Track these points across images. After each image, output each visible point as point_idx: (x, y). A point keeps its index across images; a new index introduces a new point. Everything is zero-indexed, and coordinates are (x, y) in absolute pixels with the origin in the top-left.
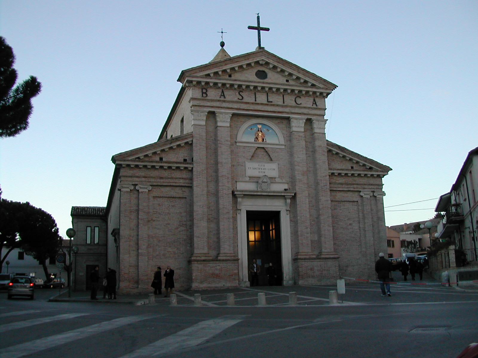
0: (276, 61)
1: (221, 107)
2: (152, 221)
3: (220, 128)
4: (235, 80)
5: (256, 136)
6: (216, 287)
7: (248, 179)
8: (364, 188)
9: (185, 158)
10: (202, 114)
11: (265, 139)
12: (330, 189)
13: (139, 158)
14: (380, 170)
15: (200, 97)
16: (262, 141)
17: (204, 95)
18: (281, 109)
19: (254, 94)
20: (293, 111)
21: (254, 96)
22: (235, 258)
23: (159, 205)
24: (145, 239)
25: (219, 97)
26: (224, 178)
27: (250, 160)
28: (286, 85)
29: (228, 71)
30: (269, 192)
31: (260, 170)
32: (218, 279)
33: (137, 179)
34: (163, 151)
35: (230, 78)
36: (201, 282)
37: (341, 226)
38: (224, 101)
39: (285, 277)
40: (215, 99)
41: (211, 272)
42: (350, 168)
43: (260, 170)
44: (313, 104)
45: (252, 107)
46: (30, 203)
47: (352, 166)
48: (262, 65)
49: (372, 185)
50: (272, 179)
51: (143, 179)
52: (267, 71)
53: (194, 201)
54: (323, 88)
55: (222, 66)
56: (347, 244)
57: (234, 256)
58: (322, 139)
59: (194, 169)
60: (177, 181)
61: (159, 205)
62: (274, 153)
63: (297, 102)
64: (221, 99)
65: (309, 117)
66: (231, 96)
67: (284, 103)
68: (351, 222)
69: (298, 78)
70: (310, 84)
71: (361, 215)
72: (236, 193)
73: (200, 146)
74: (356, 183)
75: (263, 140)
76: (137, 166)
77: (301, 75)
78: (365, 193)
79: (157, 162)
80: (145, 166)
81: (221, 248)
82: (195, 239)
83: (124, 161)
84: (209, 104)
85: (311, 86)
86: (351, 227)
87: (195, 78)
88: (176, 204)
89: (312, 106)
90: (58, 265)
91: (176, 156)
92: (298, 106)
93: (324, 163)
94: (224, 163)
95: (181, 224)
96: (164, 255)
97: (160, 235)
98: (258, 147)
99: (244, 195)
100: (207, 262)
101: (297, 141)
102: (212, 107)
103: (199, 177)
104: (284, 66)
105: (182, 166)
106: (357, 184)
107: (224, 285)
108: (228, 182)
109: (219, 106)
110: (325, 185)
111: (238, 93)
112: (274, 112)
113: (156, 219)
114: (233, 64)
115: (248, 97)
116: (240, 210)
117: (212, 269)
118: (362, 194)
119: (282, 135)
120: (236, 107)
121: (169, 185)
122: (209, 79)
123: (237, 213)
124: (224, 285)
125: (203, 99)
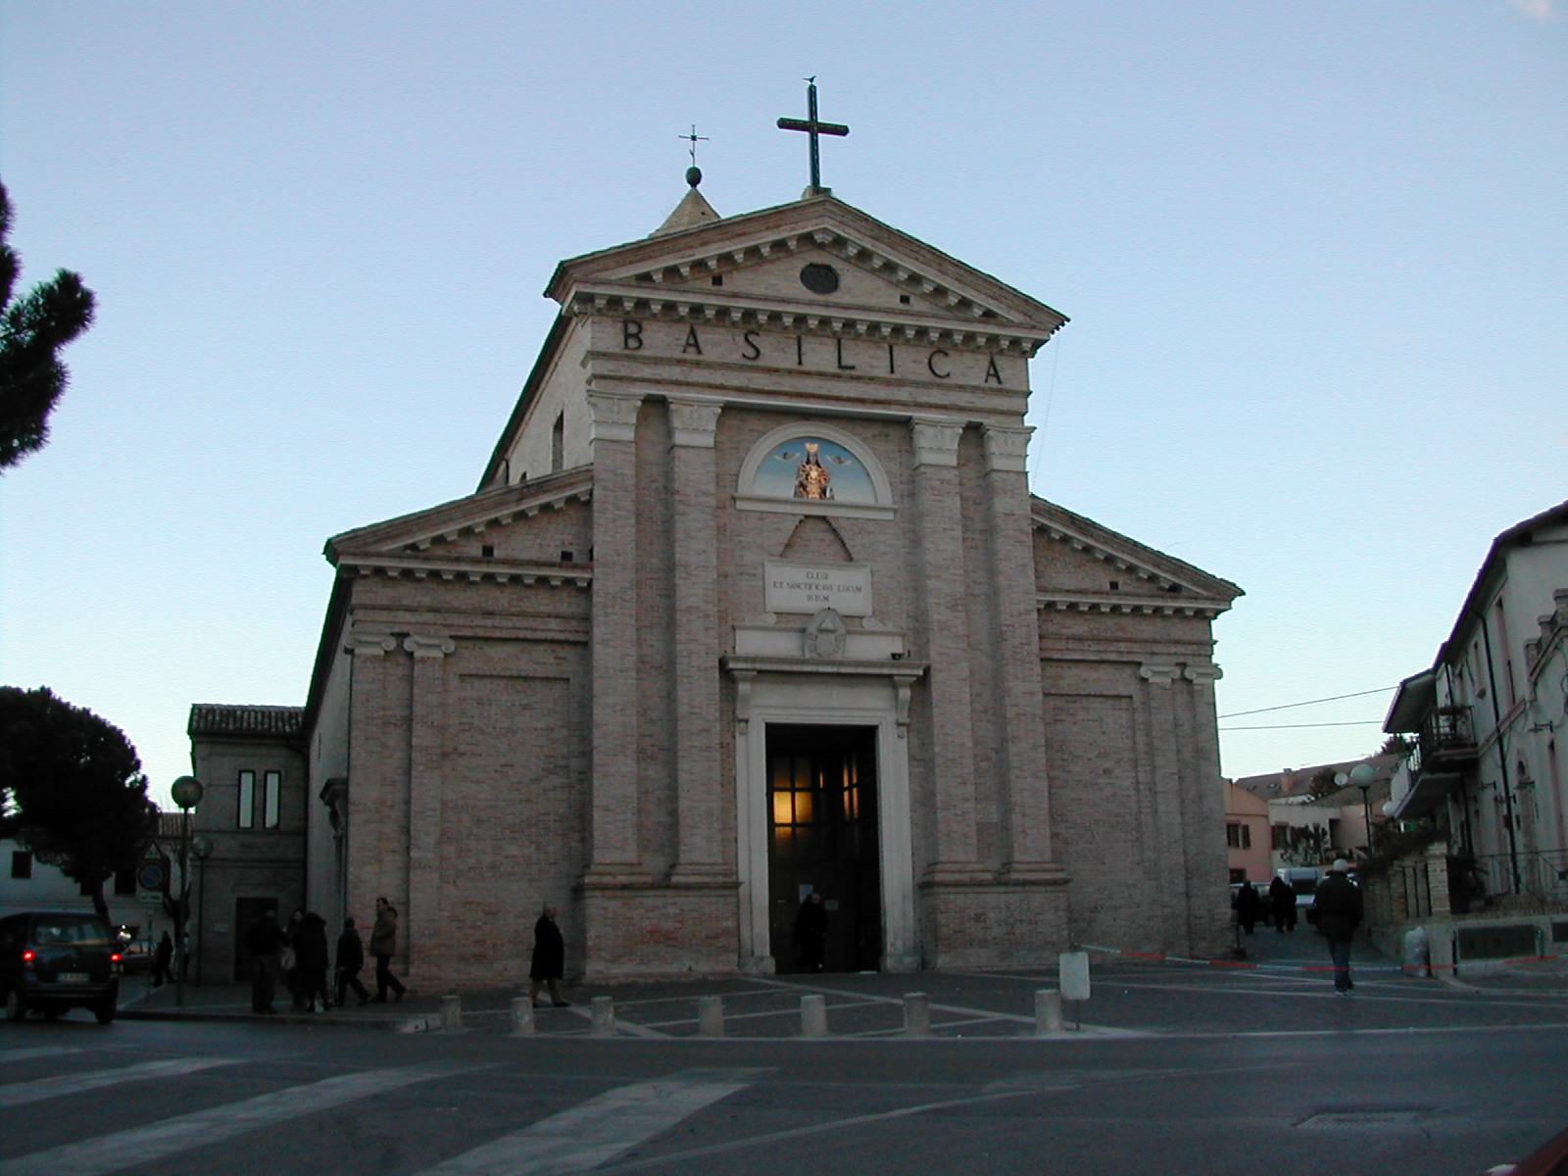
1: (688, 384)
4: (735, 296)
5: (801, 479)
6: (662, 975)
7: (771, 620)
8: (1153, 654)
9: (565, 549)
10: (624, 404)
11: (831, 490)
13: (414, 547)
14: (1204, 593)
16: (821, 497)
17: (633, 343)
18: (883, 393)
20: (922, 399)
23: (480, 703)
28: (902, 313)
29: (713, 264)
33: (408, 617)
34: (494, 524)
35: (716, 288)
36: (615, 959)
38: (698, 364)
42: (1108, 587)
44: (988, 375)
45: (788, 384)
47: (1115, 580)
48: (821, 246)
49: (1177, 642)
51: (428, 617)
52: (837, 265)
54: (1019, 326)
55: (692, 247)
58: (1016, 491)
60: (538, 623)
63: (937, 372)
67: (892, 372)
69: (940, 291)
70: (978, 312)
71: (1141, 739)
72: (731, 665)
74: (1128, 635)
75: (824, 492)
76: (407, 574)
78: (1156, 669)
79: (474, 561)
83: (367, 555)
84: (647, 372)
85: (983, 318)
87: (602, 287)
92: (939, 381)
96: (493, 867)
98: (807, 517)
99: (760, 672)
102: (658, 382)
103: (610, 610)
104: (893, 252)
105: (557, 574)
106: (1130, 640)
107: (690, 969)
109: (681, 378)
110: (1024, 641)
111: (742, 338)
113: (468, 748)
115: (776, 352)
116: (747, 721)
117: (650, 914)
118: (1144, 672)
120: (736, 383)
121: (513, 636)
122: (648, 291)
125: (628, 357)
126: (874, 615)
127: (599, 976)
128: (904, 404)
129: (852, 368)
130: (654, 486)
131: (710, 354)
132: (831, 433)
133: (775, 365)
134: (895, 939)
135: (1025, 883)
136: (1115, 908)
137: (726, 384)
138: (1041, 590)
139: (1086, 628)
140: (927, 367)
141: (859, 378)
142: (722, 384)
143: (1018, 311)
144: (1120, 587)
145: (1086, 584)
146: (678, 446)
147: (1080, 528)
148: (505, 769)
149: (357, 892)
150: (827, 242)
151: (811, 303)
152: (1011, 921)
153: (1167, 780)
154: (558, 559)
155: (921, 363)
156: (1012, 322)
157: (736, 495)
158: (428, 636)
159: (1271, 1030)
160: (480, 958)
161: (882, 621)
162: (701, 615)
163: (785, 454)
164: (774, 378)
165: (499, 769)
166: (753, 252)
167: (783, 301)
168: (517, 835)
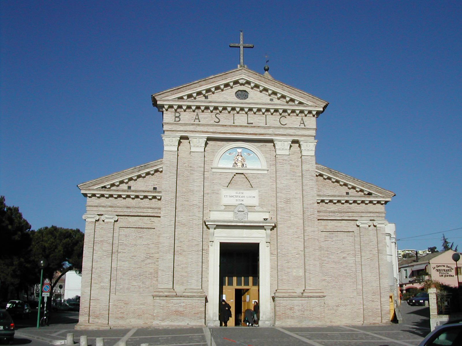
0: (257, 79)
1: (196, 131)
4: (210, 102)
5: (235, 161)
6: (178, 326)
7: (223, 208)
9: (154, 187)
10: (174, 139)
11: (246, 164)
12: (318, 218)
13: (104, 187)
14: (380, 195)
15: (172, 122)
16: (242, 167)
18: (262, 131)
22: (201, 295)
23: (126, 236)
26: (195, 208)
27: (226, 187)
29: (204, 92)
30: (245, 222)
31: (237, 198)
32: (181, 317)
33: (103, 209)
34: (130, 179)
35: (206, 100)
36: (163, 320)
37: (332, 260)
38: (198, 125)
39: (262, 317)
40: (189, 122)
41: (174, 308)
42: (345, 194)
43: (238, 198)
45: (229, 130)
46: (80, 229)
47: (348, 191)
49: (371, 212)
50: (251, 208)
51: (110, 209)
54: (311, 106)
55: (196, 87)
56: (340, 280)
57: (201, 293)
58: (310, 162)
60: (145, 210)
61: (126, 236)
62: (255, 179)
65: (296, 138)
66: (207, 120)
69: (283, 97)
70: (297, 102)
71: (357, 247)
74: (352, 211)
75: (243, 165)
76: (103, 196)
78: (362, 222)
79: (124, 191)
80: (355, 202)
83: (89, 190)
84: (182, 128)
85: (299, 105)
86: (345, 261)
87: (166, 102)
88: (143, 235)
91: (146, 184)
92: (283, 126)
93: (311, 188)
94: (195, 191)
96: (128, 289)
97: (124, 267)
98: (237, 173)
99: (217, 225)
100: (171, 298)
101: (281, 166)
102: (185, 131)
103: (167, 206)
104: (266, 84)
107: (188, 324)
108: (199, 211)
109: (193, 130)
110: (312, 213)
113: (122, 250)
114: (209, 85)
115: (225, 118)
118: (358, 223)
119: (265, 159)
120: (211, 130)
123: (209, 245)
124: (188, 324)
126: (261, 205)
127: (157, 325)
129: (252, 124)
132: (239, 144)
134: (263, 315)
135: (308, 297)
138: (319, 195)
139: (336, 209)
142: (207, 131)
144: (350, 193)
145: (337, 193)
150: (244, 83)
151: (237, 103)
152: (303, 310)
153: (366, 261)
155: (277, 121)
160: (122, 318)
161: (262, 208)
162: (197, 207)
163: (230, 153)
164: (225, 128)
166: (217, 88)
168: (136, 279)
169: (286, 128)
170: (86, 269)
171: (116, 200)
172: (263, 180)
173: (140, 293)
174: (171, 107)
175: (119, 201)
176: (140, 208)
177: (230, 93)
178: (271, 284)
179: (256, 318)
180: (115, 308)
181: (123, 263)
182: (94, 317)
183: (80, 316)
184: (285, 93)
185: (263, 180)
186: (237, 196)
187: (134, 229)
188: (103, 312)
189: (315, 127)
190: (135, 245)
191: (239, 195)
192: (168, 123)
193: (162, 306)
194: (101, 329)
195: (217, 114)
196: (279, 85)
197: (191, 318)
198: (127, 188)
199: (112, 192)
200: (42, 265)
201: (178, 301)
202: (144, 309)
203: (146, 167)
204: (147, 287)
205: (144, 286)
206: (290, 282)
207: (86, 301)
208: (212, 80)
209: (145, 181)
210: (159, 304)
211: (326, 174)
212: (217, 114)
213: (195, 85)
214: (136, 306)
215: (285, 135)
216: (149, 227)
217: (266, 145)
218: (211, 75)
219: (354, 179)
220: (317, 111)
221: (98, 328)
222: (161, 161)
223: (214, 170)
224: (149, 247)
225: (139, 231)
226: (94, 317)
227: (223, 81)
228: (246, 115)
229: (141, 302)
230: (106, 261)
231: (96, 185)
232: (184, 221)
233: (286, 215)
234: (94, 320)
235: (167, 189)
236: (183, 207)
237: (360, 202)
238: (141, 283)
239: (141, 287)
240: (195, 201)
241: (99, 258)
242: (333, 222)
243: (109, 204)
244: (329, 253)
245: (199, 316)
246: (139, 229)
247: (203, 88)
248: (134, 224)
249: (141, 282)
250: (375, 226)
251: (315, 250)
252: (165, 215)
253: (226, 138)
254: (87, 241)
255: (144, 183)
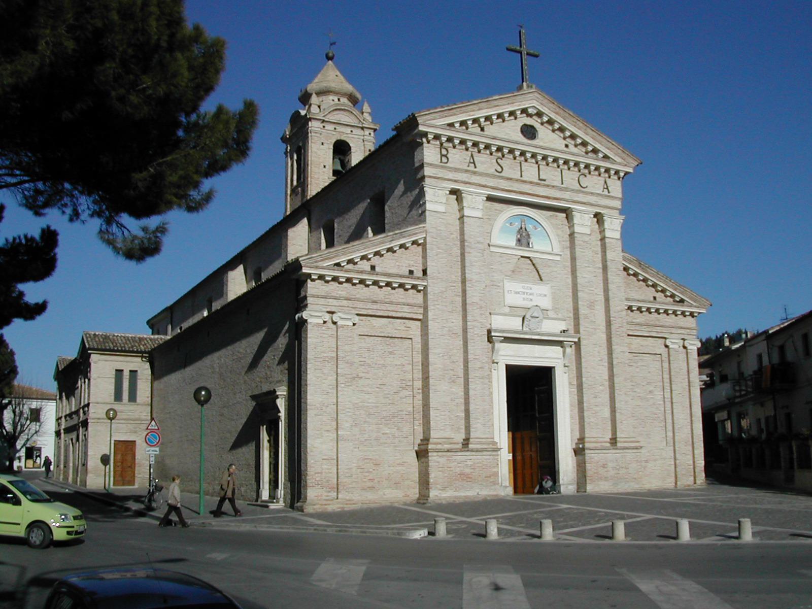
0: (554, 110)
1: (470, 183)
2: (357, 379)
3: (468, 219)
8: (671, 333)
13: (338, 265)
14: (694, 304)
17: (444, 160)
18: (558, 194)
19: (519, 164)
20: (576, 199)
21: (519, 168)
24: (348, 410)
25: (467, 164)
26: (475, 308)
28: (565, 153)
32: (469, 483)
33: (335, 302)
35: (482, 133)
36: (444, 489)
38: (475, 173)
39: (562, 479)
41: (458, 470)
43: (525, 296)
44: (604, 188)
45: (516, 186)
48: (530, 115)
49: (682, 328)
51: (345, 303)
52: (537, 126)
53: (430, 347)
54: (620, 164)
55: (474, 111)
59: (429, 289)
60: (399, 308)
63: (582, 185)
64: (469, 168)
65: (456, 186)
66: (485, 166)
67: (562, 184)
68: (651, 388)
69: (584, 144)
70: (601, 155)
72: (493, 334)
73: (439, 248)
74: (661, 324)
76: (335, 279)
77: (589, 138)
80: (349, 280)
81: (472, 430)
82: (431, 413)
83: (317, 267)
84: (451, 175)
87: (433, 128)
88: (394, 348)
89: (603, 191)
90: (149, 451)
91: (397, 263)
95: (404, 385)
96: (377, 439)
97: (369, 403)
98: (522, 257)
99: (505, 338)
102: (455, 181)
103: (436, 303)
105: (409, 282)
106: (662, 326)
111: (495, 161)
112: (548, 198)
113: (363, 375)
115: (510, 167)
116: (497, 363)
117: (460, 465)
118: (668, 343)
120: (492, 184)
121: (386, 315)
122: (454, 132)
125: (442, 167)
126: (555, 309)
127: (436, 498)
128: (567, 201)
129: (545, 180)
130: (453, 236)
131: (480, 169)
132: (523, 210)
133: (510, 176)
136: (655, 460)
137: (488, 184)
138: (627, 299)
140: (577, 182)
141: (548, 186)
143: (619, 156)
146: (466, 216)
147: (643, 268)
148: (382, 386)
149: (312, 454)
152: (618, 467)
154: (407, 273)
156: (615, 161)
157: (490, 244)
158: (345, 313)
159: (707, 520)
165: (379, 386)
167: (494, 138)
168: (388, 422)
169: (587, 193)
170: (313, 407)
171: (354, 287)
172: (555, 269)
173: (396, 446)
174: (437, 137)
175: (358, 291)
176: (391, 303)
177: (513, 126)
178: (572, 430)
179: (28, 496)
180: (361, 472)
181: (367, 396)
182: (328, 490)
183: (308, 488)
184: (588, 139)
185: (555, 269)
186: (524, 293)
187: (380, 338)
188: (345, 480)
189: (620, 196)
190: (384, 365)
191: (527, 291)
192: (431, 165)
193: (441, 466)
194: (345, 509)
195: (499, 158)
196: (581, 124)
197: (482, 484)
198: (369, 267)
199: (353, 273)
200: (202, 399)
201: (463, 458)
202: (403, 472)
203: (402, 235)
204: (405, 436)
205: (400, 434)
206: (599, 427)
207: (316, 461)
208: (496, 103)
209: (396, 258)
210: (437, 464)
211: (634, 268)
212: (499, 158)
213: (471, 107)
214: (392, 468)
215: (584, 203)
216: (404, 336)
217: (556, 216)
218: (495, 94)
219: (667, 278)
220: (449, 136)
221: (342, 508)
222: (424, 227)
223: (492, 249)
224: (404, 369)
225: (388, 343)
226: (328, 490)
227: (509, 106)
228: (537, 165)
229: (399, 461)
230: (345, 393)
231: (327, 261)
232: (455, 328)
233: (590, 327)
234: (329, 494)
235: (435, 274)
236: (454, 305)
237: (357, 282)
238: (395, 430)
239: (397, 435)
240: (474, 298)
241: (331, 387)
242: (639, 340)
243: (344, 294)
244: (633, 384)
245: (491, 481)
246: (388, 339)
247: (483, 113)
248: (381, 330)
249: (396, 428)
250: (335, 323)
251: (626, 379)
252: (435, 317)
253: (494, 197)
254: (313, 357)
255: (394, 261)
